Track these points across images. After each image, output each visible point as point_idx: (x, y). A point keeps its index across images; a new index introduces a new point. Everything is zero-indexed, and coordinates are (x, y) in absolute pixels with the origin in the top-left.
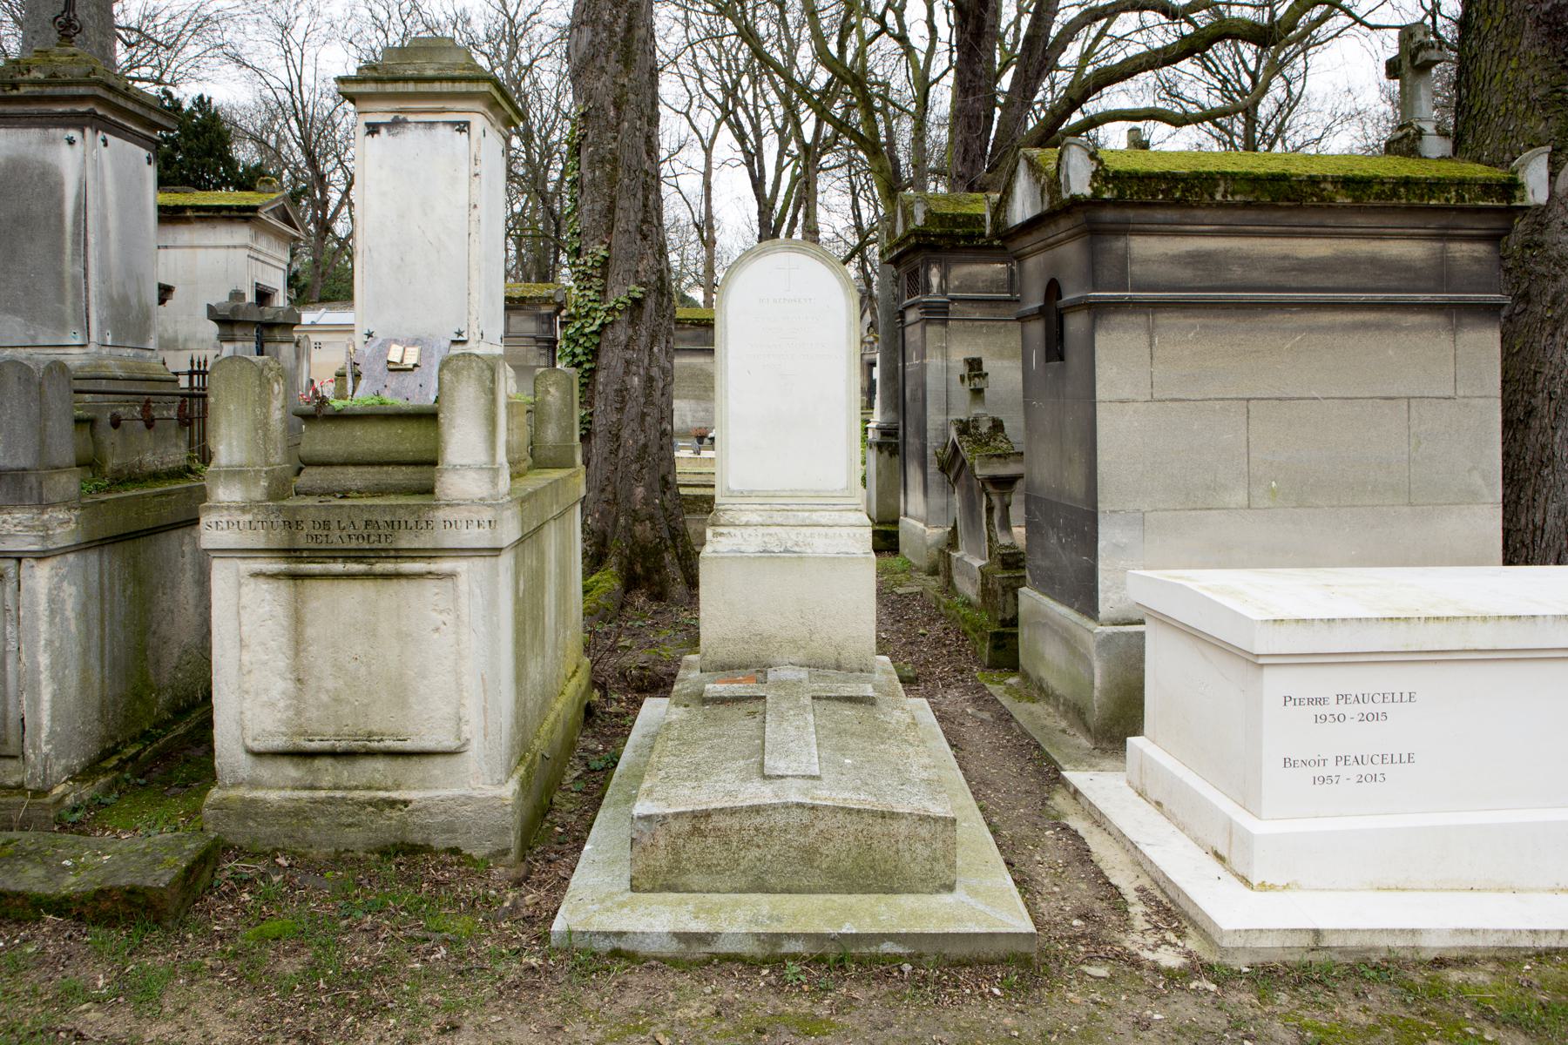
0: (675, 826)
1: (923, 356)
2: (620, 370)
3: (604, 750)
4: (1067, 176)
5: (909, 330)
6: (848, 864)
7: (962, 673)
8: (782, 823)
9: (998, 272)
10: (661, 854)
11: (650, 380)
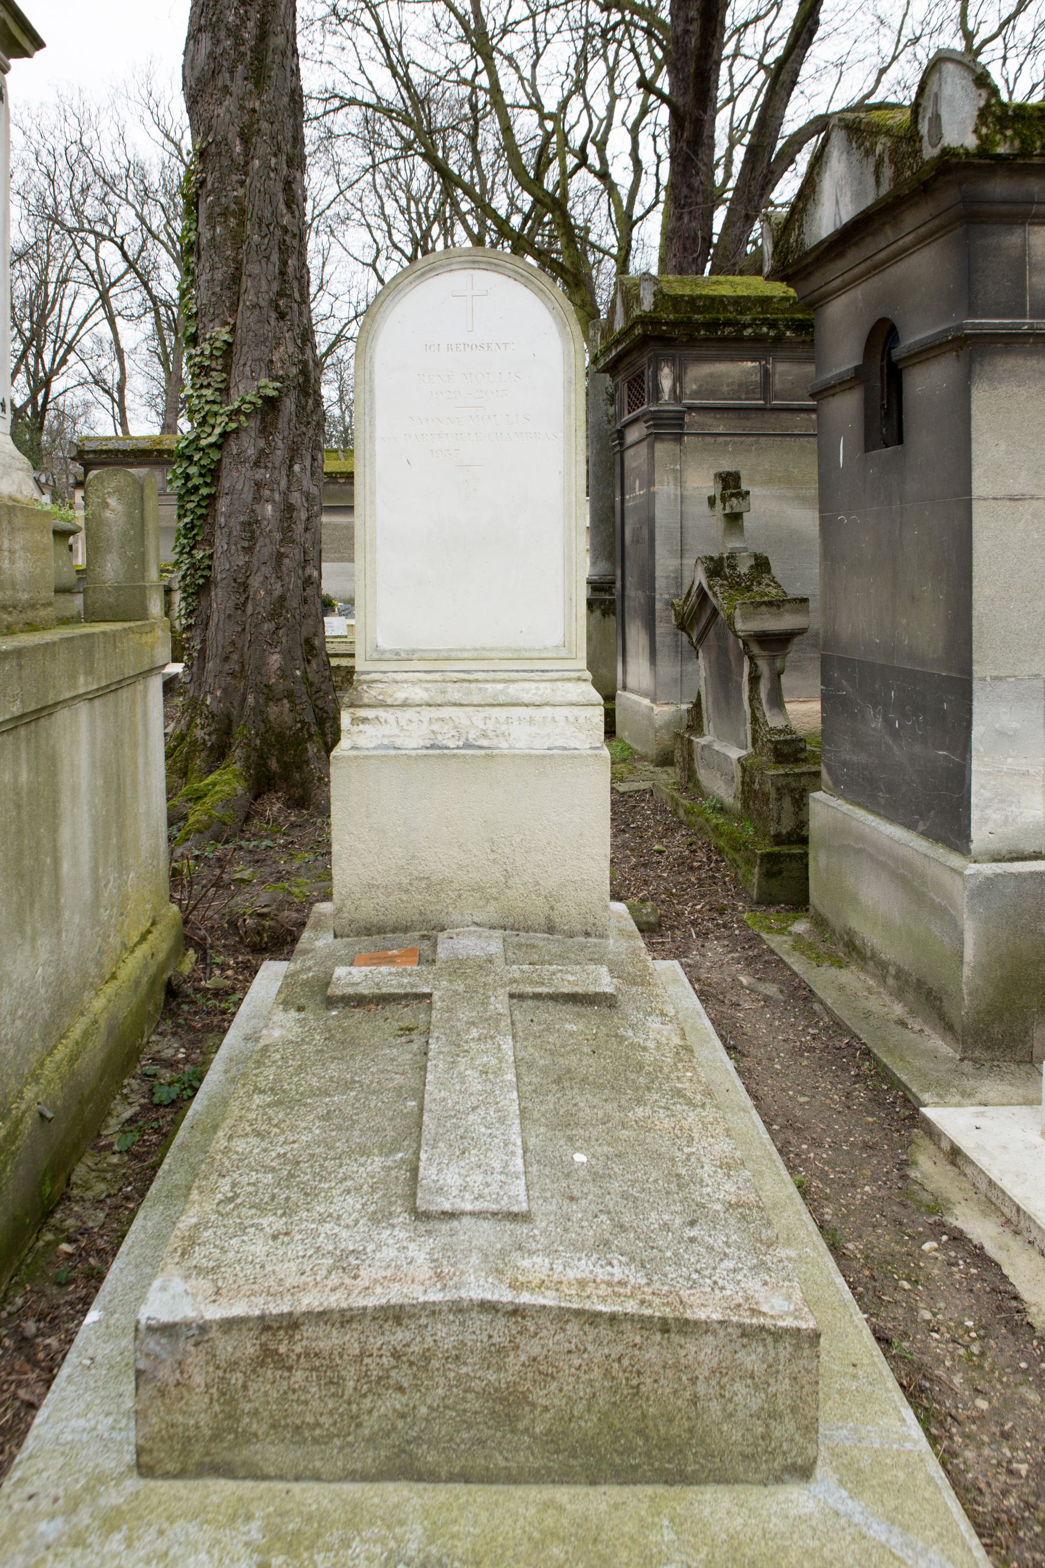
0: (226, 1347)
1: (651, 482)
2: (248, 496)
3: (187, 1060)
4: (936, 118)
5: (629, 453)
6: (589, 1424)
7: (721, 913)
8: (449, 1344)
9: (748, 373)
10: (198, 1401)
11: (289, 509)
